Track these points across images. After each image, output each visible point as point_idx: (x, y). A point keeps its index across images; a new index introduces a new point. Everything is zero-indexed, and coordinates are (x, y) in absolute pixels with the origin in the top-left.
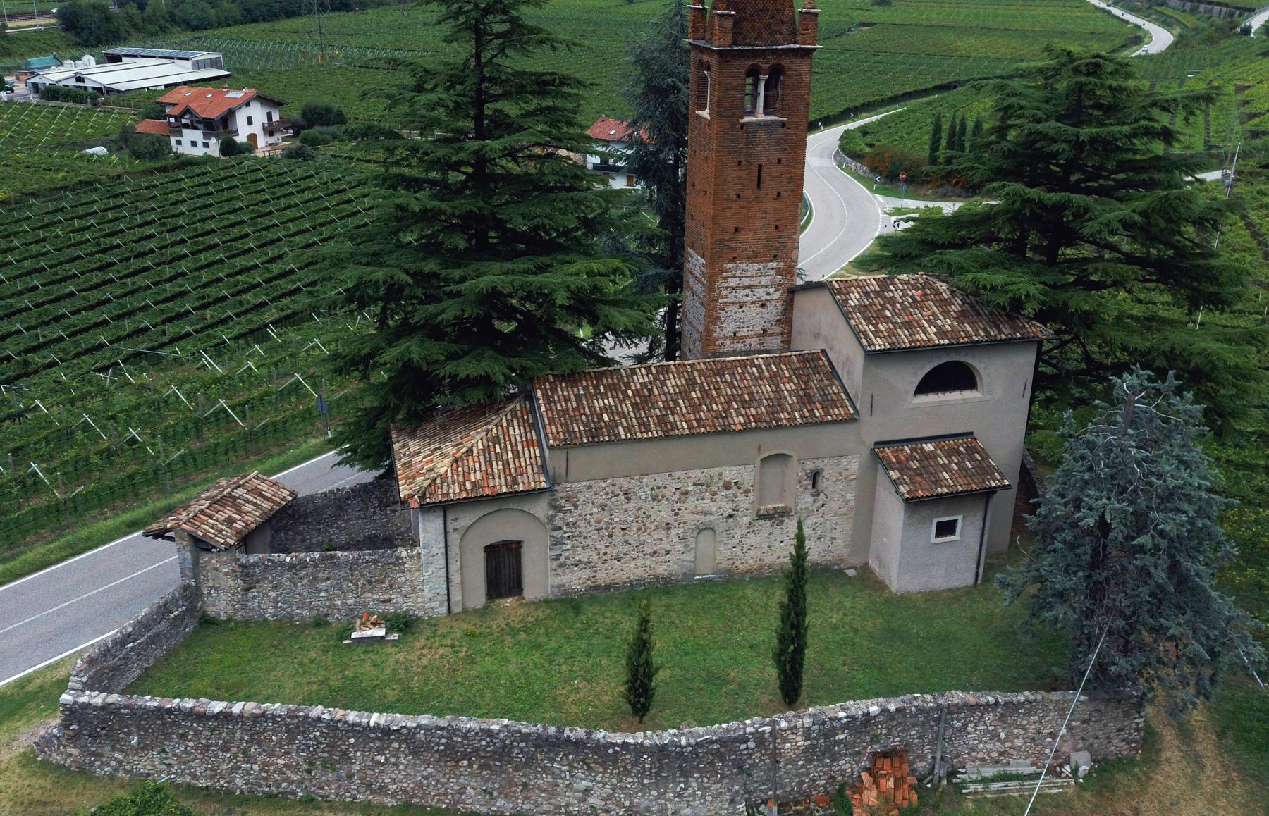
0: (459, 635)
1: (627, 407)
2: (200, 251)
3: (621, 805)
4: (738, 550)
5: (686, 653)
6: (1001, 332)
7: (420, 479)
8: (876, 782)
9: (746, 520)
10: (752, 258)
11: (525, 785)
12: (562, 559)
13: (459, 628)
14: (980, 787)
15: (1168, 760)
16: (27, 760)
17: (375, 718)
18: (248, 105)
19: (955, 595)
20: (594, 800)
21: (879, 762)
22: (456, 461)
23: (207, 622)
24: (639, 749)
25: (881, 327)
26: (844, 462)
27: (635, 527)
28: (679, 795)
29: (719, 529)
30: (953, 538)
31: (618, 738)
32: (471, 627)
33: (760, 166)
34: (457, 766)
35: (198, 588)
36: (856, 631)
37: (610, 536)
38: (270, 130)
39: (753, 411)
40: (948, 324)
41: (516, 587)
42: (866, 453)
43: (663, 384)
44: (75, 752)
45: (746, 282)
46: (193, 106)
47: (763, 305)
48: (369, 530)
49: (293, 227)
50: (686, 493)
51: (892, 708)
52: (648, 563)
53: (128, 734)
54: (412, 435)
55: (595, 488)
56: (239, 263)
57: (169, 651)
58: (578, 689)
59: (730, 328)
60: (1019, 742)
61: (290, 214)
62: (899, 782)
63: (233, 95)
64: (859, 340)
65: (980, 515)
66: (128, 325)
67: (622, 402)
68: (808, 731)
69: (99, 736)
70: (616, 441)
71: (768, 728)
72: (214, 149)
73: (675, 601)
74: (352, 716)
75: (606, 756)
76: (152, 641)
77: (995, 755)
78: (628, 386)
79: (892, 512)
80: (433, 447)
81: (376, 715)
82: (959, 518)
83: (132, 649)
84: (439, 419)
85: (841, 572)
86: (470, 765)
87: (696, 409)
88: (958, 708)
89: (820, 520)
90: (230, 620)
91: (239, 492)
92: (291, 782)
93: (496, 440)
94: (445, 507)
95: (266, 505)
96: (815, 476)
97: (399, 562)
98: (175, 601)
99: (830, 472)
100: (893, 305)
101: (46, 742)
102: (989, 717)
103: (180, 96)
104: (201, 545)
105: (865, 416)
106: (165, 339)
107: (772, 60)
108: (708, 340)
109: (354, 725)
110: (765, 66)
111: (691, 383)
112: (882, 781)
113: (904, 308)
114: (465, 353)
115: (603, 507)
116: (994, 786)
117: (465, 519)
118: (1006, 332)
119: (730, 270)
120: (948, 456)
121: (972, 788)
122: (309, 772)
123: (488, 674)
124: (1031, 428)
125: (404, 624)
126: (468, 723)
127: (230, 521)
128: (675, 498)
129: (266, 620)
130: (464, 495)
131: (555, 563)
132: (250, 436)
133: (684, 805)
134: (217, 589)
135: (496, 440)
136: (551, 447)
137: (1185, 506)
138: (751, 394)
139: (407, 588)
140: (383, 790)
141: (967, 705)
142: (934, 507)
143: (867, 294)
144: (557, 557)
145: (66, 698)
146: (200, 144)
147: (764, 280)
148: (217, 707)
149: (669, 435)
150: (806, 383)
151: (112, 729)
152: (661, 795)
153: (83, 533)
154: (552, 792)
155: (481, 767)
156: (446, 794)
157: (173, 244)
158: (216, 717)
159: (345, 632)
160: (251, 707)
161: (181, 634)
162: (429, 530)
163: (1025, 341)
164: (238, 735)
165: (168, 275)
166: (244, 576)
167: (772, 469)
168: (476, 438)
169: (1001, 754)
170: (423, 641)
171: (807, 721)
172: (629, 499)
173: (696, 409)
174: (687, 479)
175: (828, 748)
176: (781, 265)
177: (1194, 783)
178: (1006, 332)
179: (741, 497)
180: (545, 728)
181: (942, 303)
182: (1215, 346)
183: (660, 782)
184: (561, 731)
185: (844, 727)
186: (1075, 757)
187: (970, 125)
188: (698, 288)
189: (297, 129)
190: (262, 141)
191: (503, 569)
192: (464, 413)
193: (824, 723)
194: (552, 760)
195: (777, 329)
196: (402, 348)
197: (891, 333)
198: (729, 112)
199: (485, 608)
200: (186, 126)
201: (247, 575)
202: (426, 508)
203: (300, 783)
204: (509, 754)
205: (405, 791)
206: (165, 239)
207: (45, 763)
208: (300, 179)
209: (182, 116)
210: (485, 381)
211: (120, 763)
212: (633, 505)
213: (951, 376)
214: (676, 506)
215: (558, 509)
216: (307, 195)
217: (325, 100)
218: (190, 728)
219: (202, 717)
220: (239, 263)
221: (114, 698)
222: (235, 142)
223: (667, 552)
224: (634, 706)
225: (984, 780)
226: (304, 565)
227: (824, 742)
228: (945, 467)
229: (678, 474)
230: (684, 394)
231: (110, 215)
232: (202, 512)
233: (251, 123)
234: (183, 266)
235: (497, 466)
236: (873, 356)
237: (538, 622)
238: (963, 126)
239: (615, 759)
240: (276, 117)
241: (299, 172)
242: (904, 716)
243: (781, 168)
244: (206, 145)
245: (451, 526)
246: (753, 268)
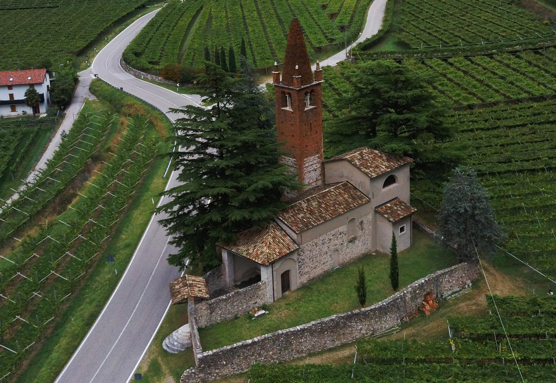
1: (308, 215)
3: (370, 330)
8: (428, 303)
9: (346, 244)
11: (344, 334)
17: (298, 328)
20: (363, 332)
28: (385, 321)
42: (373, 211)
44: (202, 375)
45: (310, 163)
69: (211, 366)
74: (292, 329)
82: (405, 225)
85: (371, 255)
88: (440, 275)
90: (206, 327)
96: (362, 223)
110: (309, 91)
115: (310, 251)
116: (453, 296)
122: (280, 353)
124: (411, 191)
129: (218, 323)
134: (201, 316)
149: (326, 221)
154: (351, 333)
155: (331, 333)
156: (320, 346)
158: (250, 345)
174: (326, 237)
177: (496, 280)
181: (381, 157)
182: (455, 152)
195: (320, 178)
203: (277, 358)
211: (217, 374)
213: (391, 180)
219: (247, 345)
221: (215, 351)
225: (449, 295)
226: (230, 298)
235: (281, 245)
238: (223, 53)
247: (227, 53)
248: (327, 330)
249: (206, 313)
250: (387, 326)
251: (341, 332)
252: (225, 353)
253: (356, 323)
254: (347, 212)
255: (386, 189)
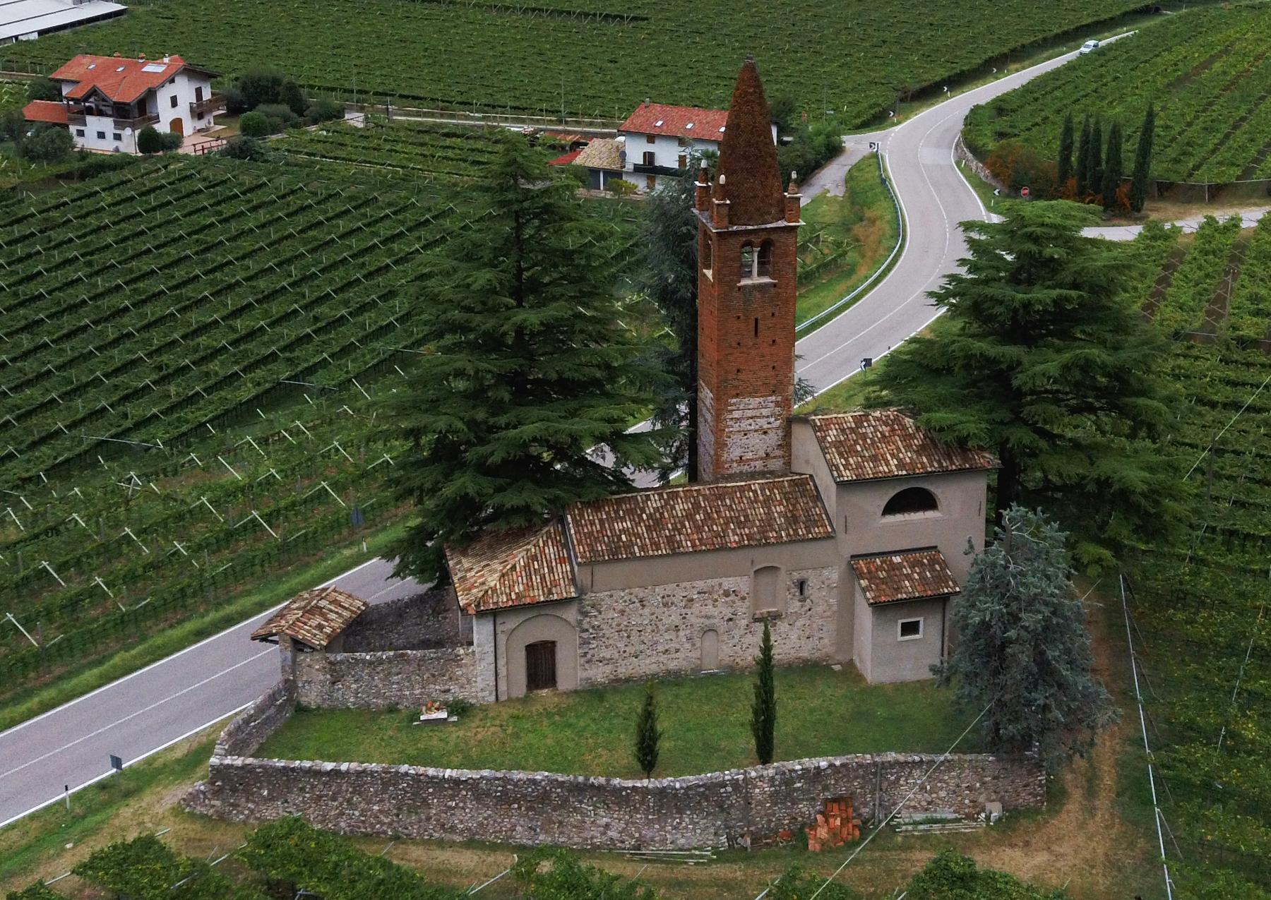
0: (506, 717)
1: (642, 530)
2: (144, 302)
3: (632, 837)
4: (738, 648)
5: (689, 730)
6: (952, 463)
7: (475, 591)
8: (827, 821)
9: (744, 622)
10: (753, 394)
11: (561, 823)
12: (589, 656)
13: (505, 712)
14: (910, 828)
15: (1068, 812)
16: (177, 811)
17: (448, 773)
18: (172, 81)
19: (921, 685)
21: (829, 805)
22: (503, 575)
23: (301, 710)
24: (645, 791)
25: (851, 461)
26: (826, 573)
27: (649, 629)
28: (675, 828)
29: (721, 630)
30: (917, 636)
31: (629, 783)
32: (516, 712)
33: (756, 320)
34: (510, 809)
35: (294, 681)
36: (830, 713)
37: (628, 637)
38: (198, 112)
39: (747, 531)
40: (907, 456)
41: (551, 681)
42: (844, 565)
43: (673, 508)
44: (218, 803)
45: (750, 413)
46: (100, 85)
47: (765, 433)
48: (423, 634)
49: (253, 265)
50: (692, 600)
51: (838, 763)
52: (661, 659)
53: (260, 788)
54: (464, 553)
55: (613, 598)
56: (195, 318)
57: (276, 732)
58: (601, 756)
59: (735, 453)
60: (943, 794)
61: (246, 245)
62: (845, 821)
63: (150, 68)
64: (831, 471)
65: (939, 617)
66: (81, 406)
67: (638, 524)
68: (772, 779)
70: (632, 558)
71: (741, 777)
72: (129, 143)
73: (684, 691)
74: (431, 771)
75: (620, 798)
76: (266, 722)
77: (924, 803)
78: (643, 511)
79: (865, 616)
80: (483, 564)
81: (448, 771)
82: (921, 619)
83: (254, 727)
84: (486, 539)
85: (828, 667)
86: (519, 808)
87: (699, 529)
89: (808, 622)
90: (319, 708)
91: (323, 603)
92: (383, 824)
93: (534, 558)
94: (495, 614)
95: (346, 614)
96: (801, 585)
97: (457, 660)
98: (279, 691)
99: (813, 582)
100: (865, 440)
101: (194, 797)
102: (916, 773)
103: (81, 70)
104: (299, 646)
105: (841, 535)
106: (128, 424)
107: (764, 236)
108: (718, 463)
109: (433, 777)
111: (697, 506)
112: (831, 820)
113: (873, 442)
114: (510, 485)
115: (622, 612)
117: (511, 623)
118: (958, 463)
119: (734, 404)
120: (912, 567)
121: (904, 828)
123: (531, 745)
125: (461, 709)
126: (518, 775)
127: (320, 627)
128: (683, 604)
129: (348, 708)
130: (510, 603)
131: (583, 660)
132: (284, 547)
133: (679, 836)
134: (309, 682)
135: (534, 558)
136: (579, 564)
137: (1043, 608)
138: (746, 516)
139: (463, 680)
140: (453, 829)
141: (897, 762)
142: (899, 610)
143: (843, 430)
144: (586, 653)
145: (214, 760)
146: (109, 136)
147: (765, 412)
148: (329, 766)
150: (794, 506)
151: (248, 784)
152: (662, 828)
153: (159, 640)
154: (580, 827)
155: (528, 809)
157: (110, 291)
158: (328, 773)
159: (415, 716)
160: (354, 765)
161: (286, 716)
162: (482, 632)
163: (974, 471)
164: (344, 788)
165: (111, 337)
166: (332, 671)
167: (765, 579)
168: (519, 557)
169: (929, 803)
170: (477, 722)
171: (771, 772)
172: (643, 606)
173: (699, 529)
175: (789, 794)
176: (779, 399)
177: (1082, 826)
178: (958, 463)
179: (739, 603)
180: (575, 777)
181: (907, 437)
183: (661, 819)
184: (587, 779)
185: (800, 778)
186: (989, 806)
187: (1106, 129)
188: (708, 416)
189: (234, 110)
190: (189, 127)
191: (541, 665)
192: (507, 535)
193: (784, 773)
194: (581, 802)
195: (778, 453)
196: (459, 482)
197: (859, 466)
198: (727, 279)
199: (526, 696)
200: (90, 111)
201: (335, 671)
202: (481, 614)
203: (390, 824)
204: (549, 797)
205: (469, 829)
206: (95, 286)
207: (192, 815)
208: (251, 190)
209: (86, 99)
210: (526, 510)
211: (252, 811)
212: (646, 611)
213: (912, 498)
214: (684, 611)
215: (585, 614)
216: (262, 215)
217: (272, 68)
218: (308, 782)
219: (318, 774)
220: (195, 318)
222: (158, 135)
223: (677, 651)
224: (642, 762)
225: (916, 823)
226: (381, 662)
227: (785, 789)
228: (908, 577)
229: (685, 584)
230: (689, 516)
231: (20, 250)
232: (298, 620)
233: (176, 104)
234: (130, 323)
235: (536, 580)
236: (842, 485)
237: (569, 708)
238: (1098, 132)
239: (627, 799)
240: (207, 95)
241: (247, 180)
242: (848, 770)
243: (774, 320)
244: (118, 137)
245: (499, 629)
246: (755, 402)
247: (1105, 137)
248: (516, 800)
249: (322, 678)
250: (682, 841)
251: (555, 816)
252: (272, 774)
253: (596, 808)
254: (749, 546)
255: (890, 519)
